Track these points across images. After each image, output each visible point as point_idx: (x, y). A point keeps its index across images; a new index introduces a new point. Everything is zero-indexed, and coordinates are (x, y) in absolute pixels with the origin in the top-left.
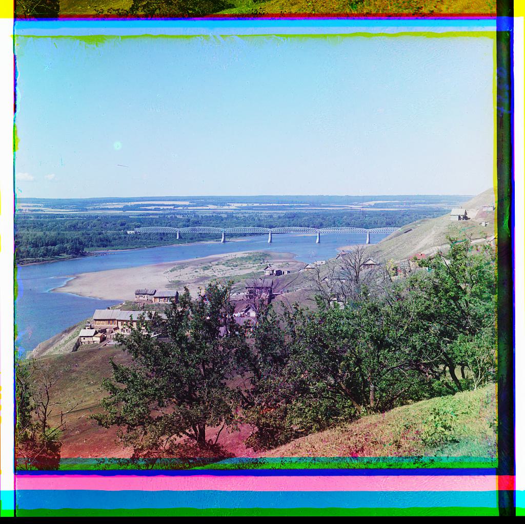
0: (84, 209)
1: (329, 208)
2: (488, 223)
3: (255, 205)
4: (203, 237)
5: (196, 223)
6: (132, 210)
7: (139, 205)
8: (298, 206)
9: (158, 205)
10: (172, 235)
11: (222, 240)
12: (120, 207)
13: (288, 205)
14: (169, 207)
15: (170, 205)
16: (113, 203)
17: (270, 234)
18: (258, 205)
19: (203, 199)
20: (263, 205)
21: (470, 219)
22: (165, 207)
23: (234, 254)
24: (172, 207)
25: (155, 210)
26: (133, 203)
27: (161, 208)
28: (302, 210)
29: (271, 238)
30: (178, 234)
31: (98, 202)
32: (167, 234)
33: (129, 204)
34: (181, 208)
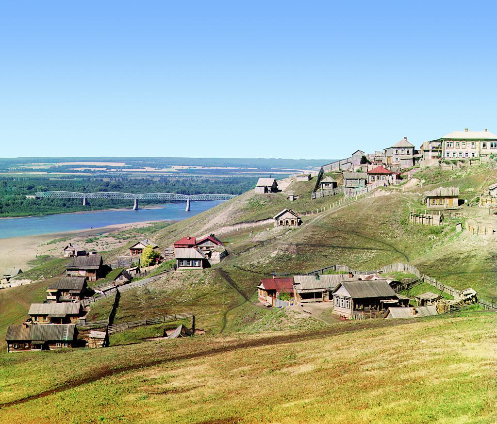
0: (5, 169)
1: (278, 173)
2: (298, 197)
3: (198, 168)
4: (114, 204)
5: (115, 187)
6: (58, 172)
7: (68, 165)
8: (243, 170)
9: (90, 166)
10: (78, 201)
11: (135, 207)
12: (46, 167)
13: (235, 168)
14: (101, 169)
15: (102, 167)
16: (39, 164)
17: (188, 202)
18: (201, 168)
19: (141, 160)
20: (206, 168)
21: (281, 191)
22: (97, 169)
23: (135, 224)
24: (104, 169)
25: (85, 171)
26: (61, 164)
27: (92, 169)
28: (249, 174)
29: (190, 205)
30: (84, 200)
31: (21, 163)
32: (73, 199)
33: (57, 165)
34: (114, 170)
